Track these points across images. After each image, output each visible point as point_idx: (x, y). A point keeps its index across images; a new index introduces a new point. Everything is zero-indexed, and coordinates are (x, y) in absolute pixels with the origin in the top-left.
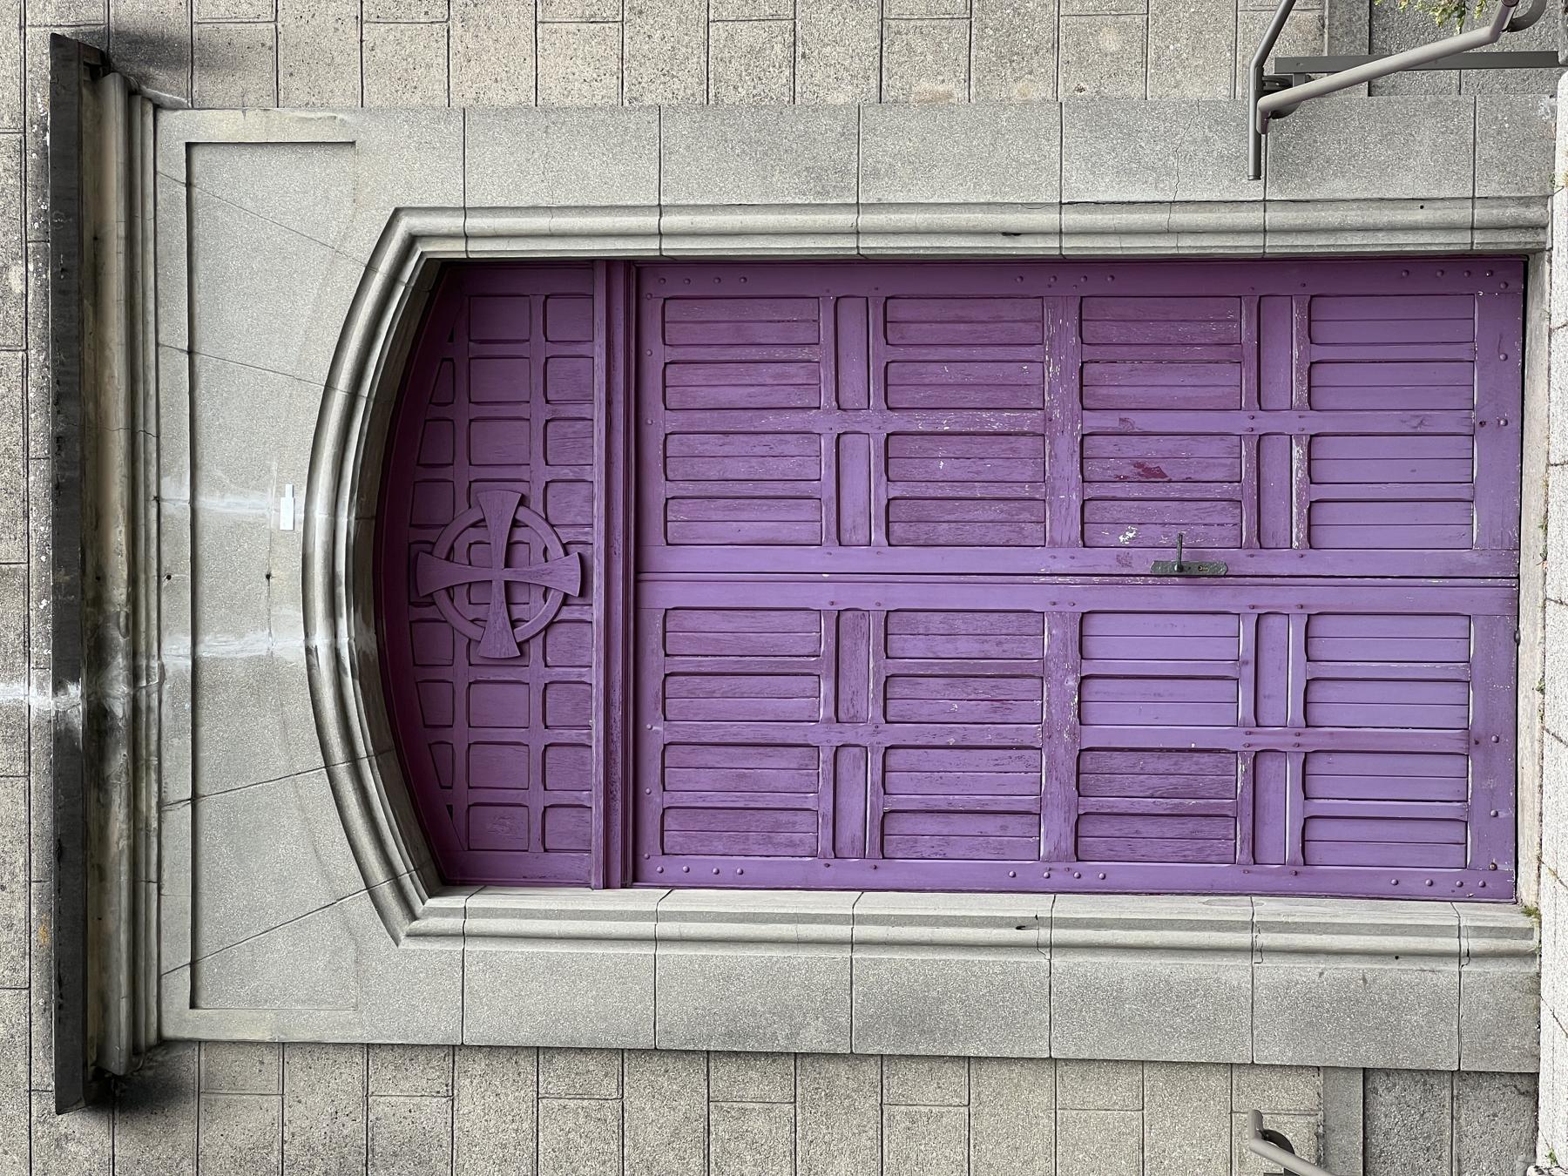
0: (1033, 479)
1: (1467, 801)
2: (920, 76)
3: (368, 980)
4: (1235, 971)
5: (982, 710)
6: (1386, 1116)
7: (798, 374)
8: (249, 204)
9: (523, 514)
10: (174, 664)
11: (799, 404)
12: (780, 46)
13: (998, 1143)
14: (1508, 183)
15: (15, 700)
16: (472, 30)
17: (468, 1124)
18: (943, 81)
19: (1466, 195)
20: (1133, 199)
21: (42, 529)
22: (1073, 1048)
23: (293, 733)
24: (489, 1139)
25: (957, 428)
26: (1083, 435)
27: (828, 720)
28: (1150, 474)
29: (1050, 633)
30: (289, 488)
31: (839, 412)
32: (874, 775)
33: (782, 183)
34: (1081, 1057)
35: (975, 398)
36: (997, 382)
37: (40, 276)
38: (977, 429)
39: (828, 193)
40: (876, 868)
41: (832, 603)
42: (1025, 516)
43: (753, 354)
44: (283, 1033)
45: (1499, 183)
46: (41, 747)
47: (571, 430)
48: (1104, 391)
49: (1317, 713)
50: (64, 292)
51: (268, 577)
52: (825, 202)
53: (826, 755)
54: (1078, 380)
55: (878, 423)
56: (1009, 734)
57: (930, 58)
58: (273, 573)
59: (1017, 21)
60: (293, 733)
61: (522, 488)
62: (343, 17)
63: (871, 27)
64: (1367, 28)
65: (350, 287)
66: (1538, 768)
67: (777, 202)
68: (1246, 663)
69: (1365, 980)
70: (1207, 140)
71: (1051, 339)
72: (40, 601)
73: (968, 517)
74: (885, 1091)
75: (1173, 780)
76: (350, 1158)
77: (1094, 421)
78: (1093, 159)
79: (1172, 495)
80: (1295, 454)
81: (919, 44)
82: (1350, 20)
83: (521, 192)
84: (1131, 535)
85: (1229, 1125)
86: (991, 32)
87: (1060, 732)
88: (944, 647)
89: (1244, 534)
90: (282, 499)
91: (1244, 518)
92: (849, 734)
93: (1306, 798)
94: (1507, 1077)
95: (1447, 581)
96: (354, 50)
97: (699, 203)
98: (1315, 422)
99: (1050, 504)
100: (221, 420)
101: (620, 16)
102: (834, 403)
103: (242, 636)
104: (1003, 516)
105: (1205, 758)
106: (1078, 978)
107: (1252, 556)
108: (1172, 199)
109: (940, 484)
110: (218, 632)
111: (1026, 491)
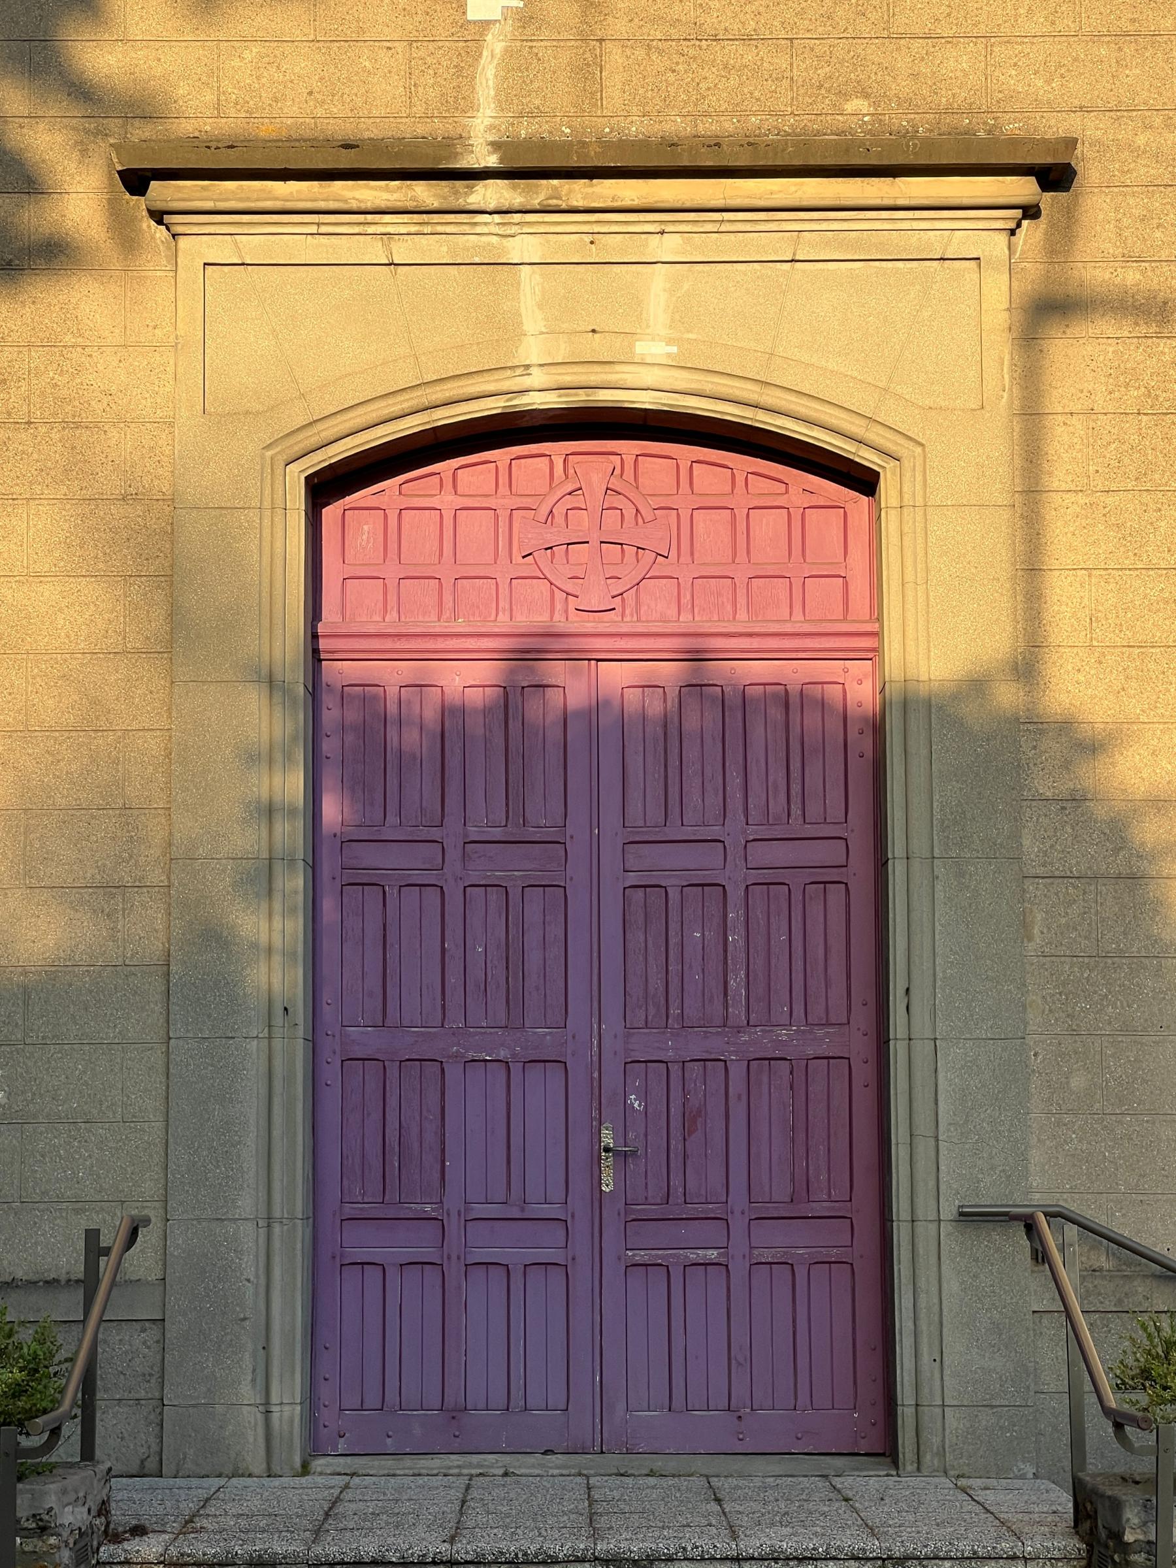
0: (685, 1017)
1: (401, 1410)
2: (1046, 913)
3: (232, 423)
4: (247, 1203)
5: (476, 973)
6: (120, 1340)
7: (778, 805)
8: (926, 314)
9: (649, 557)
10: (514, 248)
11: (751, 806)
12: (1072, 787)
13: (91, 992)
14: (957, 1437)
15: (479, 105)
16: (1083, 512)
17: (102, 513)
18: (1042, 933)
19: (946, 1400)
20: (940, 1103)
21: (634, 129)
22: (178, 1059)
23: (454, 354)
24: (88, 532)
25: (730, 948)
26: (725, 1061)
27: (466, 835)
28: (691, 1120)
29: (547, 1034)
30: (674, 349)
31: (743, 842)
32: (417, 877)
33: (951, 791)
34: (171, 1067)
35: (758, 963)
36: (772, 984)
37: (860, 127)
38: (730, 966)
39: (943, 832)
40: (334, 878)
41: (572, 837)
42: (652, 1011)
43: (795, 765)
44: (183, 346)
45: (957, 1429)
46: (439, 128)
47: (725, 600)
48: (765, 1079)
49: (479, 1274)
50: (847, 150)
51: (594, 331)
52: (935, 828)
53: (435, 833)
54: (774, 1056)
55: (735, 877)
56: (455, 998)
57: (1063, 921)
58: (597, 336)
59: (1096, 997)
60: (454, 354)
61: (673, 554)
62: (1093, 397)
63: (1090, 868)
64: (1093, 1309)
65: (853, 404)
66: (435, 1472)
67: (934, 785)
68: (523, 1210)
69: (245, 1319)
70: (993, 1168)
71: (811, 1032)
72: (569, 127)
73: (650, 959)
74: (136, 889)
75: (416, 1145)
76: (70, 408)
77: (737, 1072)
78: (974, 1067)
79: (673, 1142)
80: (710, 1252)
81: (1075, 910)
82: (1100, 1294)
83: (940, 556)
84: (636, 1105)
85: (110, 1199)
86: (1086, 975)
87: (459, 1044)
88: (533, 938)
89: (639, 1207)
90: (664, 343)
91: (653, 1207)
92: (453, 854)
93: (401, 1265)
94: (158, 1449)
95: (598, 1389)
96: (1064, 407)
97: (933, 716)
98: (739, 1269)
99: (664, 1032)
100: (733, 289)
101: (1096, 644)
102: (751, 838)
103: (540, 306)
104: (651, 990)
105: (437, 1175)
106: (242, 1062)
107: (619, 1214)
108: (940, 1138)
109: (680, 934)
110: (543, 287)
111: (674, 1011)
